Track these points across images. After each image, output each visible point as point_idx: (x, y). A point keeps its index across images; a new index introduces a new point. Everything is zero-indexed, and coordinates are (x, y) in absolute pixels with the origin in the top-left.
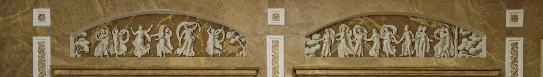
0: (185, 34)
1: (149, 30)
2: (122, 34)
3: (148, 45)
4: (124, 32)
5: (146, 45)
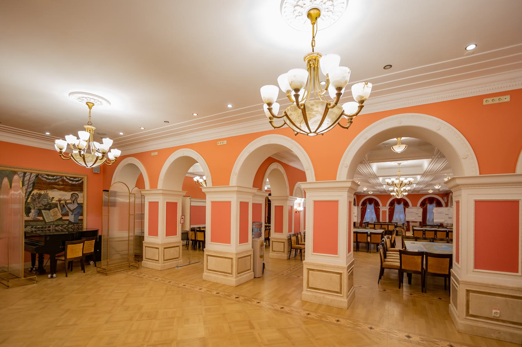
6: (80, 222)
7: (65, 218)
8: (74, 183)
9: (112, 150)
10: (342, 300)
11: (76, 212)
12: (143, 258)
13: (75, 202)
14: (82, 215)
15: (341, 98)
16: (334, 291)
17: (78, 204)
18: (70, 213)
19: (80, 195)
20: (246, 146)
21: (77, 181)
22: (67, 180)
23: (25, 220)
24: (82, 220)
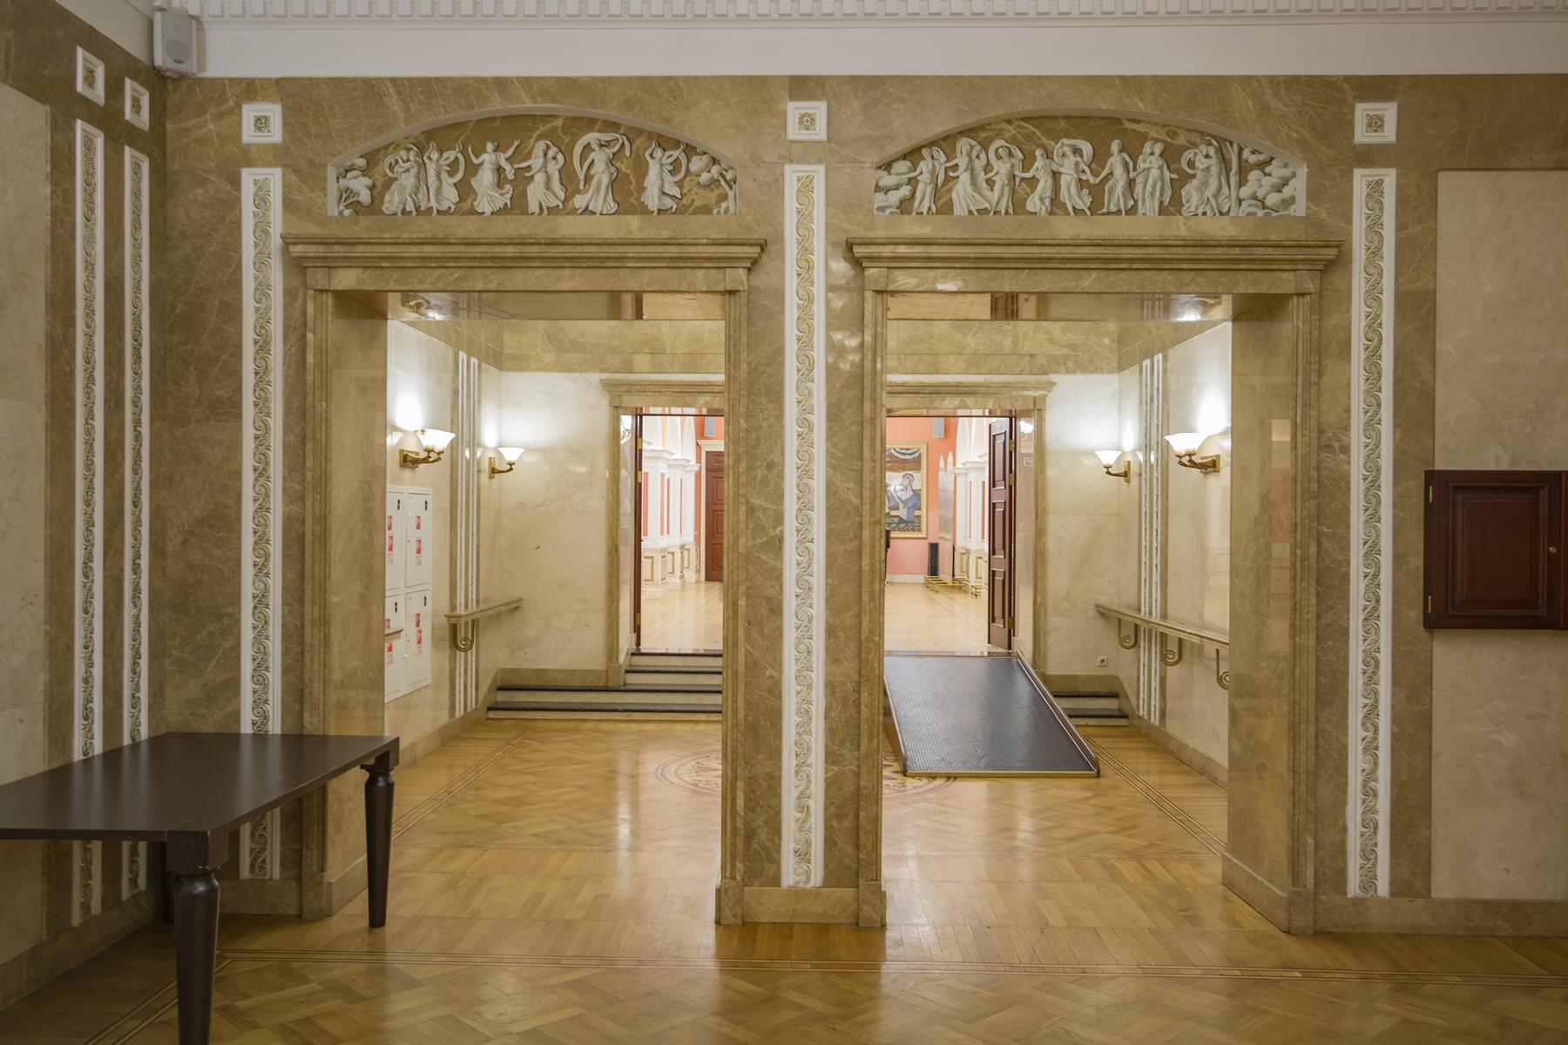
0: (593, 161)
1: (510, 152)
3: (508, 187)
4: (452, 158)
5: (503, 188)
6: (916, 520)
7: (893, 513)
8: (907, 457)
9: (330, 294)
10: (893, 534)
14: (920, 509)
15: (218, 975)
17: (913, 491)
18: (901, 506)
19: (917, 475)
21: (911, 454)
22: (896, 454)
23: (940, 546)
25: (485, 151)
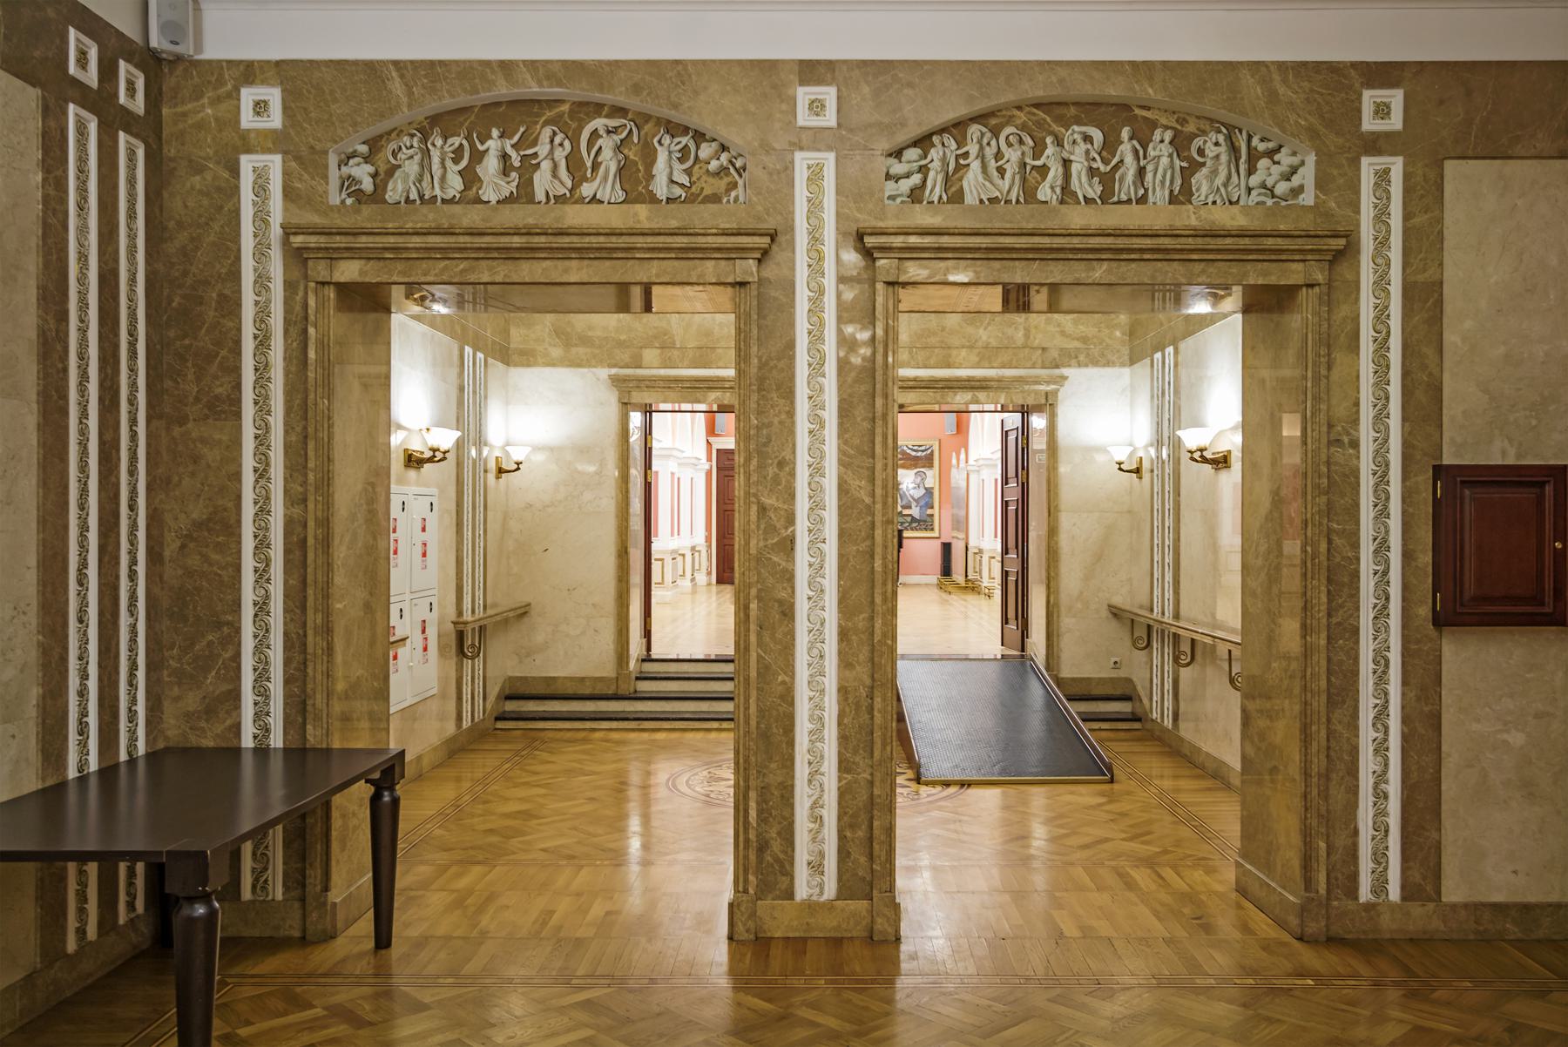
0: (601, 148)
1: (516, 138)
2: (451, 149)
3: (514, 174)
4: (457, 145)
5: (509, 176)
6: (929, 519)
7: (906, 512)
8: (919, 454)
11: (922, 503)
12: (240, 418)
13: (922, 485)
14: (932, 508)
16: (1179, 533)
17: (926, 489)
18: (914, 504)
19: (929, 473)
20: (90, 112)
21: (923, 451)
22: (909, 451)
24: (932, 515)
25: (490, 137)
